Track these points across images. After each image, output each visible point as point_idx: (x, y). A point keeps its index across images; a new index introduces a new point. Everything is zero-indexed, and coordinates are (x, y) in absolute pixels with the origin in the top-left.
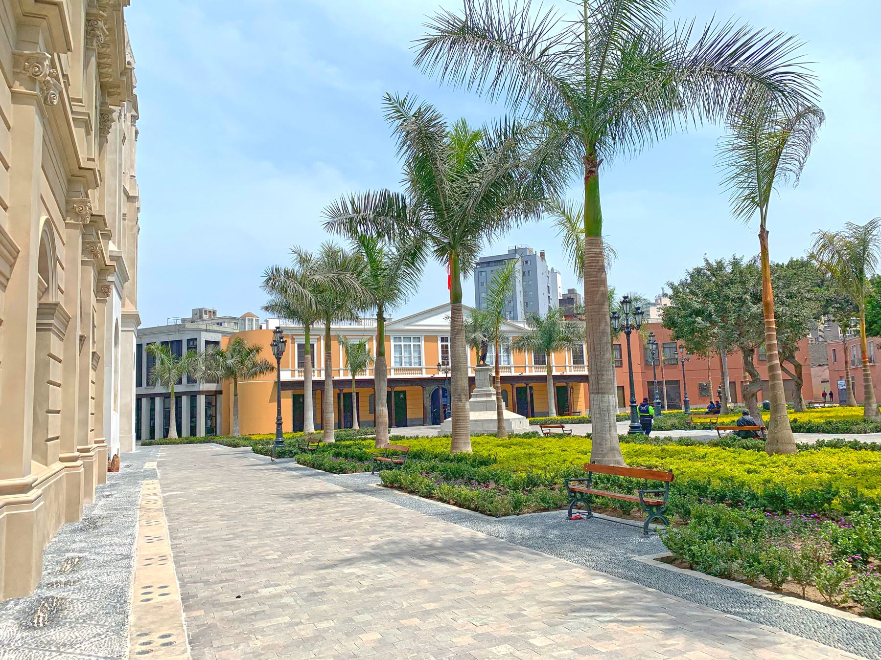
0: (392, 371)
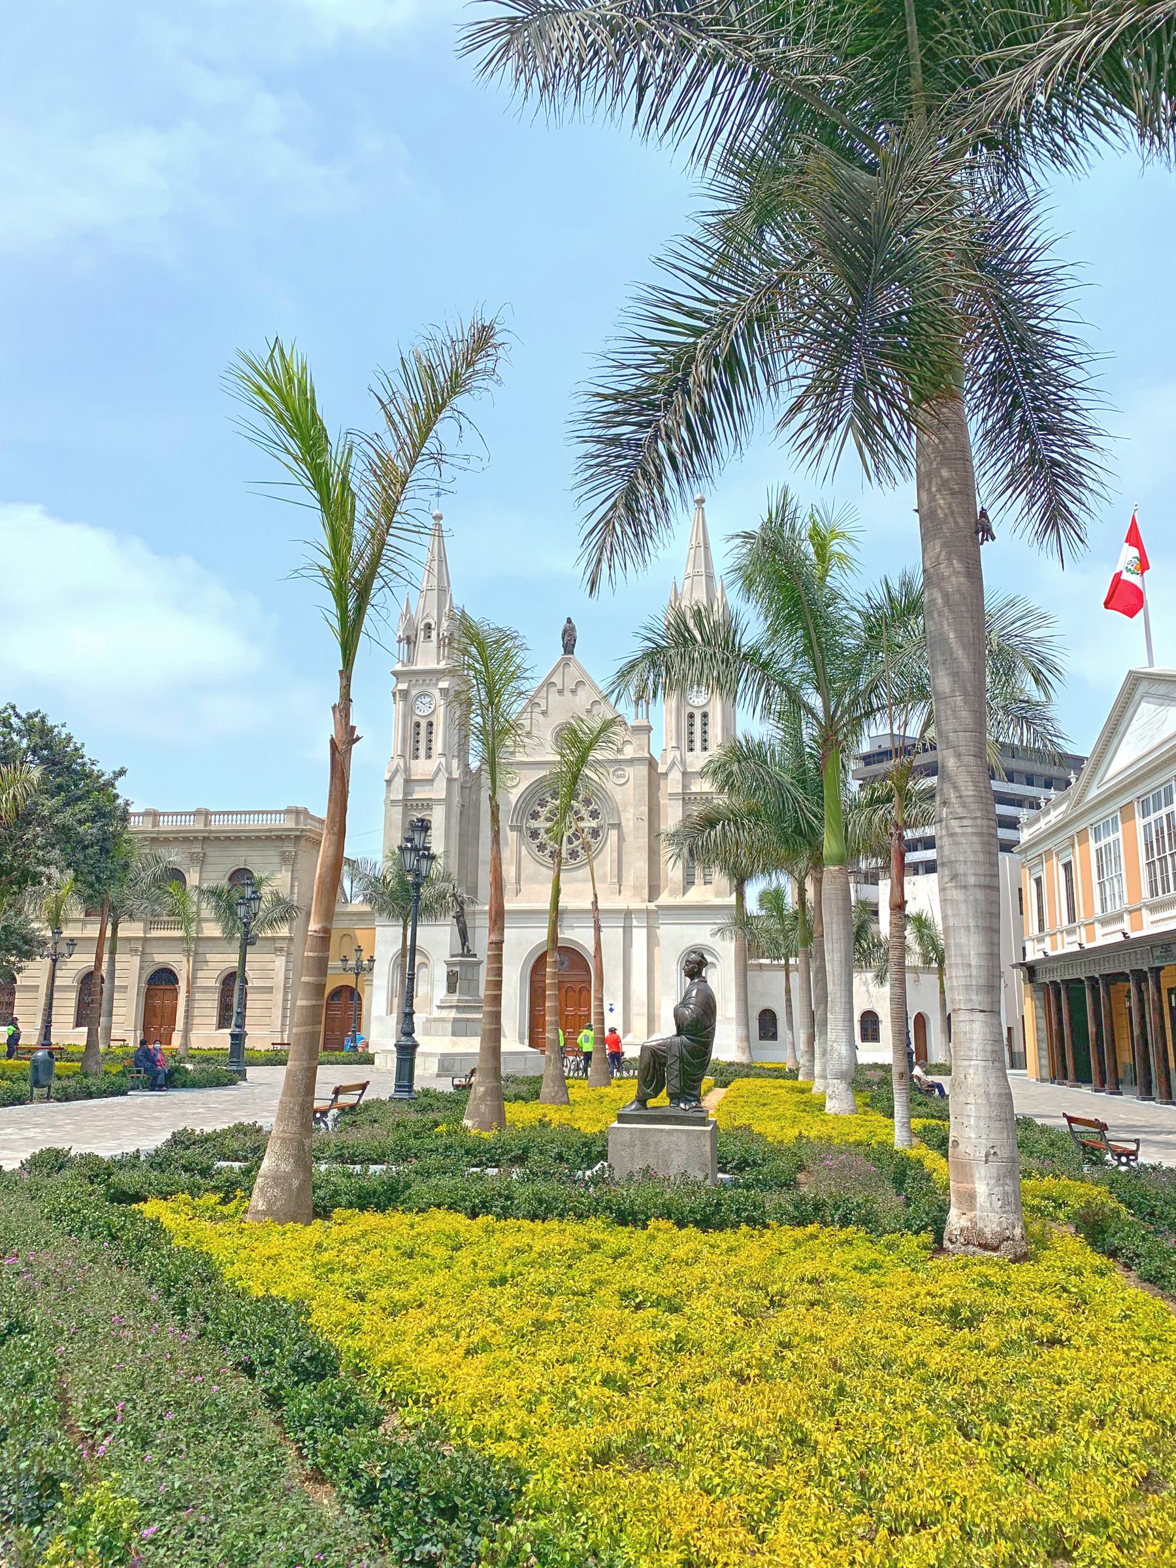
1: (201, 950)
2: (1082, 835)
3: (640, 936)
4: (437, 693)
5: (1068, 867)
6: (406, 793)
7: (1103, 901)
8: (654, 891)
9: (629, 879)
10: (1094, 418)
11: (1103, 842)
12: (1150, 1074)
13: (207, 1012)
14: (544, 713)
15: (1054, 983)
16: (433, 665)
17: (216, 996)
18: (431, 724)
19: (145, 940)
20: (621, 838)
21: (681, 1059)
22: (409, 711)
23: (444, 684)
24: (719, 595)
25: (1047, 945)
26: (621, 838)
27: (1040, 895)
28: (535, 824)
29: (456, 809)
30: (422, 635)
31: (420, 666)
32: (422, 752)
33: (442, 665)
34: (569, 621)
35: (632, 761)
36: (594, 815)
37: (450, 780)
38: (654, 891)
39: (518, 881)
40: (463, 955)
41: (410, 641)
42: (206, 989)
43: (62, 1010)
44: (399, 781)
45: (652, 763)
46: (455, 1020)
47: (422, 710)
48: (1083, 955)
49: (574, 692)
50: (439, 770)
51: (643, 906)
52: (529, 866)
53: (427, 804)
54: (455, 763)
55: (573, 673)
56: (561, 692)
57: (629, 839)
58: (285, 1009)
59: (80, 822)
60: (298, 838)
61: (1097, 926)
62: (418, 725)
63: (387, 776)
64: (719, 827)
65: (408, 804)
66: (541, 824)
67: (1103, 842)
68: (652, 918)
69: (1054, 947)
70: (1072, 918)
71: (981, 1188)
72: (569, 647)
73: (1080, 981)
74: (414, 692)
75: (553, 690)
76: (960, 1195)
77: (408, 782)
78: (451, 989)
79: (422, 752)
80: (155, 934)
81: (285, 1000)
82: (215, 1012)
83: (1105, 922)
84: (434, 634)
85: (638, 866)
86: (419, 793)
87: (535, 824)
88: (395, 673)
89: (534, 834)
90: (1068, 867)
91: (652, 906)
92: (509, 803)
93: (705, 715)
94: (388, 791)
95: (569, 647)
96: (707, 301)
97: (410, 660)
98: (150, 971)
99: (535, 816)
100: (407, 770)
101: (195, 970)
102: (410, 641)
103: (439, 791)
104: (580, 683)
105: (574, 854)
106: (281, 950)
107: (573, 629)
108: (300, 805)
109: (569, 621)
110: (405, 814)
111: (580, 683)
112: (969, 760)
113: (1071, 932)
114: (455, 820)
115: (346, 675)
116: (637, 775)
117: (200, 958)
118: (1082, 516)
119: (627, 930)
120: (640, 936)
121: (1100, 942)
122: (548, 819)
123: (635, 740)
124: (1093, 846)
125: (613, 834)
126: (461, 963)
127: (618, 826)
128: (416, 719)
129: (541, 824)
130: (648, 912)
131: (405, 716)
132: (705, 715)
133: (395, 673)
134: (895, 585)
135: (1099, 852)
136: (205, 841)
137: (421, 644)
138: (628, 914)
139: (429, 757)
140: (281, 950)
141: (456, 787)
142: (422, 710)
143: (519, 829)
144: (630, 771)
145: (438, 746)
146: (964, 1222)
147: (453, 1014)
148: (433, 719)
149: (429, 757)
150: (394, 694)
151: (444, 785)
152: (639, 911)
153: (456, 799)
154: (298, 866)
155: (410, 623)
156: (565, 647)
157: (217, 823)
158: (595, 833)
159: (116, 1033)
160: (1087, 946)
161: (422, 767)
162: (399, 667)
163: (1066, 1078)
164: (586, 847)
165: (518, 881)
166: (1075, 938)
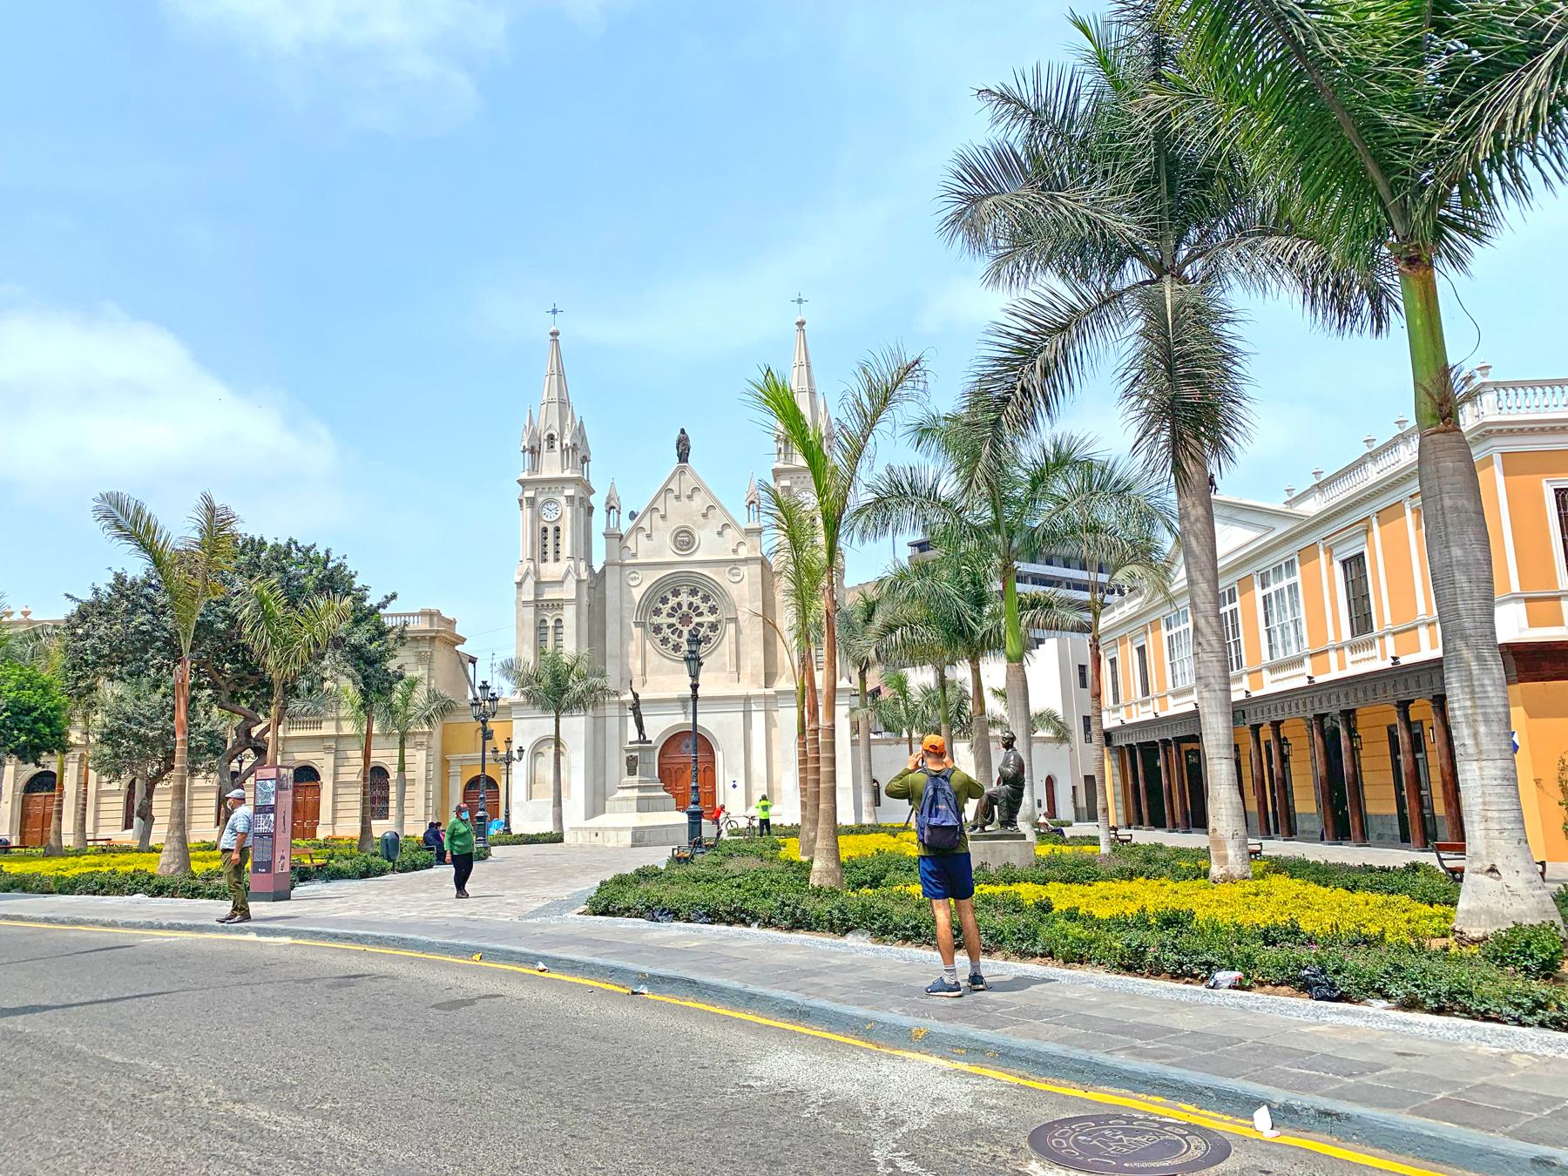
0: (1265, 673)
1: (341, 747)
2: (1155, 625)
3: (758, 719)
4: (562, 500)
5: (1141, 650)
7: (1174, 678)
8: (769, 678)
9: (747, 669)
10: (1247, 389)
11: (1174, 631)
13: (350, 805)
14: (663, 517)
15: (1130, 746)
16: (557, 474)
17: (359, 790)
18: (558, 529)
20: (738, 631)
21: (1007, 799)
22: (536, 517)
23: (570, 492)
24: (822, 409)
25: (1122, 714)
26: (738, 631)
27: (1114, 673)
28: (657, 620)
29: (585, 609)
30: (545, 445)
31: (545, 474)
32: (551, 556)
33: (567, 474)
34: (683, 431)
35: (746, 561)
36: (713, 610)
37: (579, 582)
38: (769, 678)
39: (644, 673)
40: (640, 742)
41: (534, 451)
42: (348, 784)
43: (202, 811)
44: (530, 582)
45: (764, 562)
46: (639, 798)
47: (549, 516)
48: (1157, 722)
49: (690, 497)
50: (568, 572)
51: (762, 691)
52: (654, 658)
53: (558, 605)
54: (583, 565)
55: (688, 482)
56: (678, 498)
57: (746, 631)
58: (427, 799)
59: (371, 641)
60: (433, 638)
61: (1170, 698)
62: (545, 530)
63: (518, 579)
64: (898, 632)
65: (539, 605)
66: (662, 620)
67: (1174, 631)
69: (1129, 715)
70: (1146, 692)
71: (1231, 853)
72: (683, 456)
73: (1154, 743)
74: (540, 499)
75: (671, 495)
76: (1218, 857)
77: (538, 584)
78: (631, 772)
79: (551, 556)
80: (294, 733)
81: (427, 791)
82: (358, 806)
83: (1176, 695)
84: (557, 444)
85: (754, 656)
86: (550, 594)
87: (657, 620)
88: (521, 482)
89: (658, 629)
90: (1141, 650)
91: (770, 691)
92: (632, 601)
94: (519, 593)
95: (683, 456)
96: (1028, 331)
97: (534, 468)
99: (657, 612)
100: (537, 572)
101: (336, 766)
102: (534, 451)
103: (569, 591)
104: (695, 489)
106: (422, 744)
107: (687, 439)
108: (433, 607)
109: (683, 431)
110: (536, 613)
111: (695, 489)
112: (1495, 728)
113: (1144, 703)
114: (584, 617)
116: (752, 572)
117: (341, 754)
118: (1236, 449)
119: (747, 714)
120: (758, 719)
121: (1172, 711)
122: (669, 615)
123: (747, 541)
124: (1165, 634)
125: (731, 627)
126: (640, 749)
127: (735, 620)
128: (543, 524)
129: (662, 620)
130: (766, 697)
131: (532, 522)
133: (521, 482)
134: (1050, 449)
135: (1170, 638)
138: (747, 699)
139: (557, 560)
140: (422, 744)
141: (585, 587)
142: (549, 516)
143: (643, 625)
144: (744, 570)
145: (566, 549)
146: (1222, 871)
147: (635, 793)
148: (559, 524)
149: (557, 560)
150: (521, 501)
151: (574, 586)
152: (758, 696)
153: (585, 600)
154: (434, 666)
155: (534, 435)
156: (680, 455)
160: (1161, 715)
161: (551, 570)
162: (524, 476)
163: (1141, 823)
165: (644, 673)
166: (1149, 708)
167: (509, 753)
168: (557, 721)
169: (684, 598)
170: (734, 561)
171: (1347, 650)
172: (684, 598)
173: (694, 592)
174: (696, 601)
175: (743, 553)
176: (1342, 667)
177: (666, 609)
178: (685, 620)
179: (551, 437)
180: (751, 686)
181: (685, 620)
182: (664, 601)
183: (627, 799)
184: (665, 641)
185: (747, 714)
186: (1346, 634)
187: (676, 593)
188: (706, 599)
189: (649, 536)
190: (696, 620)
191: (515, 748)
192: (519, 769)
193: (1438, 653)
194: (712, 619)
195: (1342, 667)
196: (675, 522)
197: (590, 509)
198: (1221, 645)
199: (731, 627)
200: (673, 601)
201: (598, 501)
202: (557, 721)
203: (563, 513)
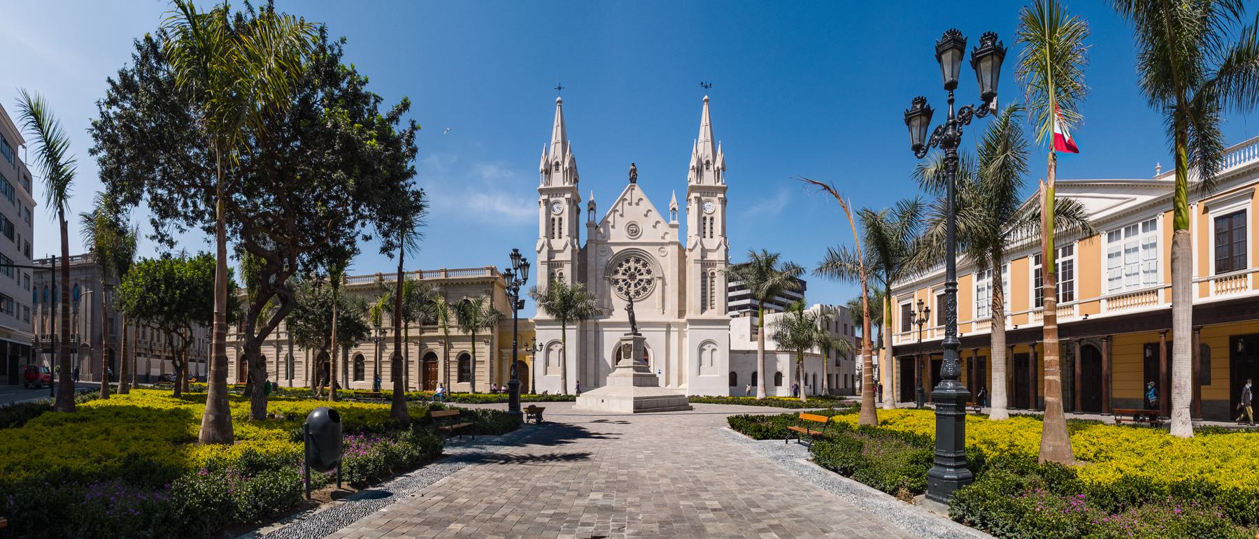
0: (1104, 302)
3: (674, 335)
6: (549, 258)
12: (460, 402)
14: (622, 215)
16: (560, 185)
19: (421, 338)
20: (664, 284)
32: (708, 234)
33: (567, 185)
36: (649, 272)
49: (637, 204)
56: (630, 204)
68: (681, 326)
79: (708, 234)
93: (712, 219)
98: (424, 353)
100: (549, 245)
105: (637, 293)
115: (61, 214)
116: (673, 251)
119: (668, 333)
127: (662, 278)
132: (712, 219)
136: (448, 286)
137: (705, 173)
144: (668, 249)
157: (452, 276)
158: (649, 282)
159: (411, 384)
164: (645, 289)
167: (534, 347)
168: (564, 330)
169: (632, 264)
170: (662, 244)
171: (1212, 282)
172: (632, 264)
173: (638, 261)
174: (639, 266)
175: (668, 239)
176: (932, 336)
177: (621, 270)
178: (632, 277)
179: (557, 164)
180: (671, 316)
181: (632, 277)
182: (621, 265)
183: (625, 376)
184: (620, 289)
185: (668, 333)
186: (1212, 272)
187: (627, 261)
188: (645, 265)
189: (622, 215)
190: (639, 277)
191: (537, 344)
192: (540, 356)
193: (1167, 306)
194: (649, 277)
195: (932, 336)
196: (627, 220)
197: (578, 211)
198: (1053, 283)
199: (659, 283)
200: (625, 266)
201: (583, 206)
202: (564, 330)
203: (563, 207)
